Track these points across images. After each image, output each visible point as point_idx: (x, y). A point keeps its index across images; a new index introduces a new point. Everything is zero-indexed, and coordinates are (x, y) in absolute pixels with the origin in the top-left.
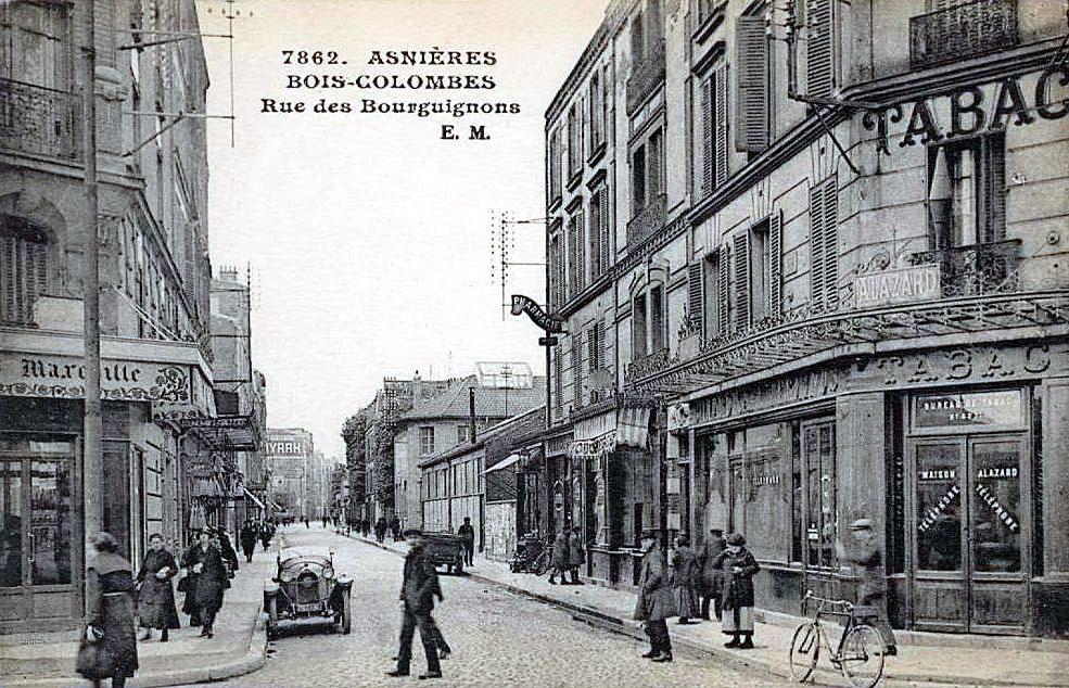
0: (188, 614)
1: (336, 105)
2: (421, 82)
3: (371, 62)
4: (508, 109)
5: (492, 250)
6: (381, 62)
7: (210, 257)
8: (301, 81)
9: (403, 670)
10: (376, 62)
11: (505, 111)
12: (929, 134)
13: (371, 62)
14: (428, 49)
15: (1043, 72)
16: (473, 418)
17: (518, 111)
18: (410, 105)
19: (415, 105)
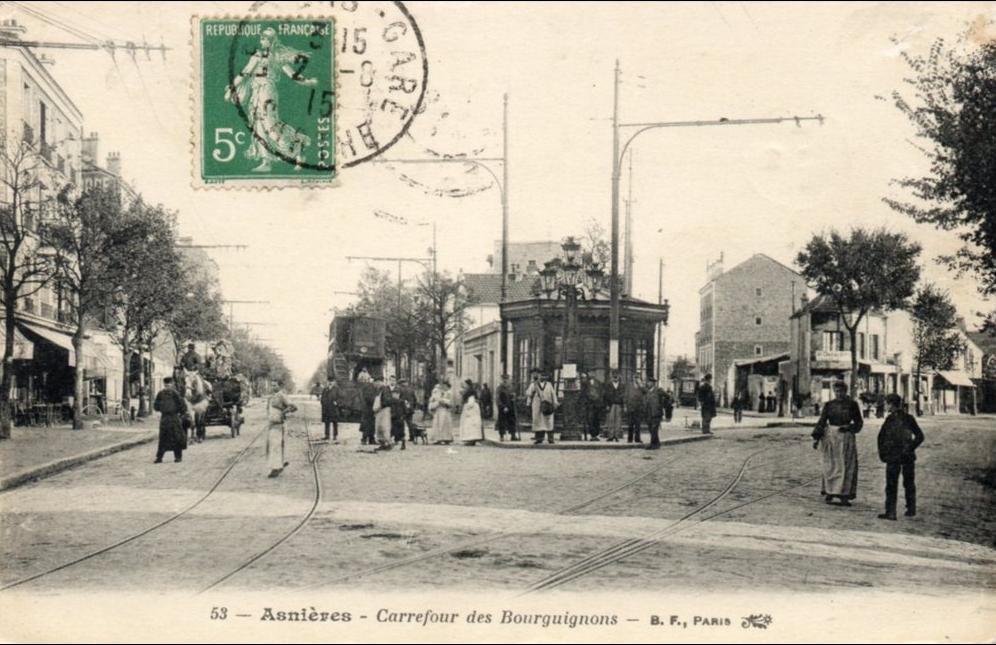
0: (884, 460)
1: (338, 614)
2: (592, 621)
3: (263, 619)
4: (288, 617)
5: (665, 618)
6: (272, 619)
7: (748, 616)
8: (513, 617)
9: (503, 621)
10: (268, 619)
11: (297, 619)
12: (782, 388)
13: (263, 619)
14: (724, 618)
15: (254, 170)
16: (41, 202)
17: (349, 619)
18: (322, 614)
19: (327, 614)
